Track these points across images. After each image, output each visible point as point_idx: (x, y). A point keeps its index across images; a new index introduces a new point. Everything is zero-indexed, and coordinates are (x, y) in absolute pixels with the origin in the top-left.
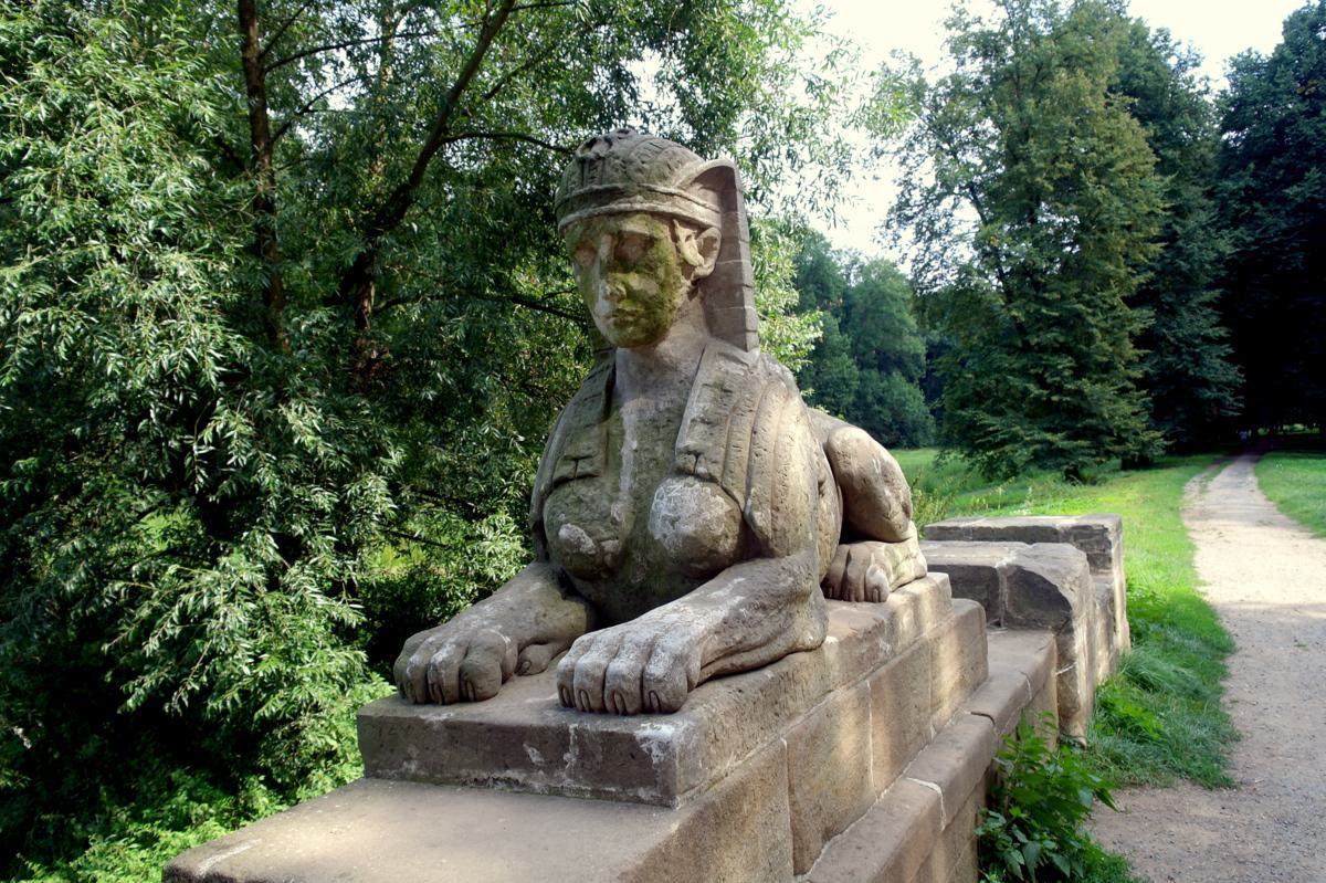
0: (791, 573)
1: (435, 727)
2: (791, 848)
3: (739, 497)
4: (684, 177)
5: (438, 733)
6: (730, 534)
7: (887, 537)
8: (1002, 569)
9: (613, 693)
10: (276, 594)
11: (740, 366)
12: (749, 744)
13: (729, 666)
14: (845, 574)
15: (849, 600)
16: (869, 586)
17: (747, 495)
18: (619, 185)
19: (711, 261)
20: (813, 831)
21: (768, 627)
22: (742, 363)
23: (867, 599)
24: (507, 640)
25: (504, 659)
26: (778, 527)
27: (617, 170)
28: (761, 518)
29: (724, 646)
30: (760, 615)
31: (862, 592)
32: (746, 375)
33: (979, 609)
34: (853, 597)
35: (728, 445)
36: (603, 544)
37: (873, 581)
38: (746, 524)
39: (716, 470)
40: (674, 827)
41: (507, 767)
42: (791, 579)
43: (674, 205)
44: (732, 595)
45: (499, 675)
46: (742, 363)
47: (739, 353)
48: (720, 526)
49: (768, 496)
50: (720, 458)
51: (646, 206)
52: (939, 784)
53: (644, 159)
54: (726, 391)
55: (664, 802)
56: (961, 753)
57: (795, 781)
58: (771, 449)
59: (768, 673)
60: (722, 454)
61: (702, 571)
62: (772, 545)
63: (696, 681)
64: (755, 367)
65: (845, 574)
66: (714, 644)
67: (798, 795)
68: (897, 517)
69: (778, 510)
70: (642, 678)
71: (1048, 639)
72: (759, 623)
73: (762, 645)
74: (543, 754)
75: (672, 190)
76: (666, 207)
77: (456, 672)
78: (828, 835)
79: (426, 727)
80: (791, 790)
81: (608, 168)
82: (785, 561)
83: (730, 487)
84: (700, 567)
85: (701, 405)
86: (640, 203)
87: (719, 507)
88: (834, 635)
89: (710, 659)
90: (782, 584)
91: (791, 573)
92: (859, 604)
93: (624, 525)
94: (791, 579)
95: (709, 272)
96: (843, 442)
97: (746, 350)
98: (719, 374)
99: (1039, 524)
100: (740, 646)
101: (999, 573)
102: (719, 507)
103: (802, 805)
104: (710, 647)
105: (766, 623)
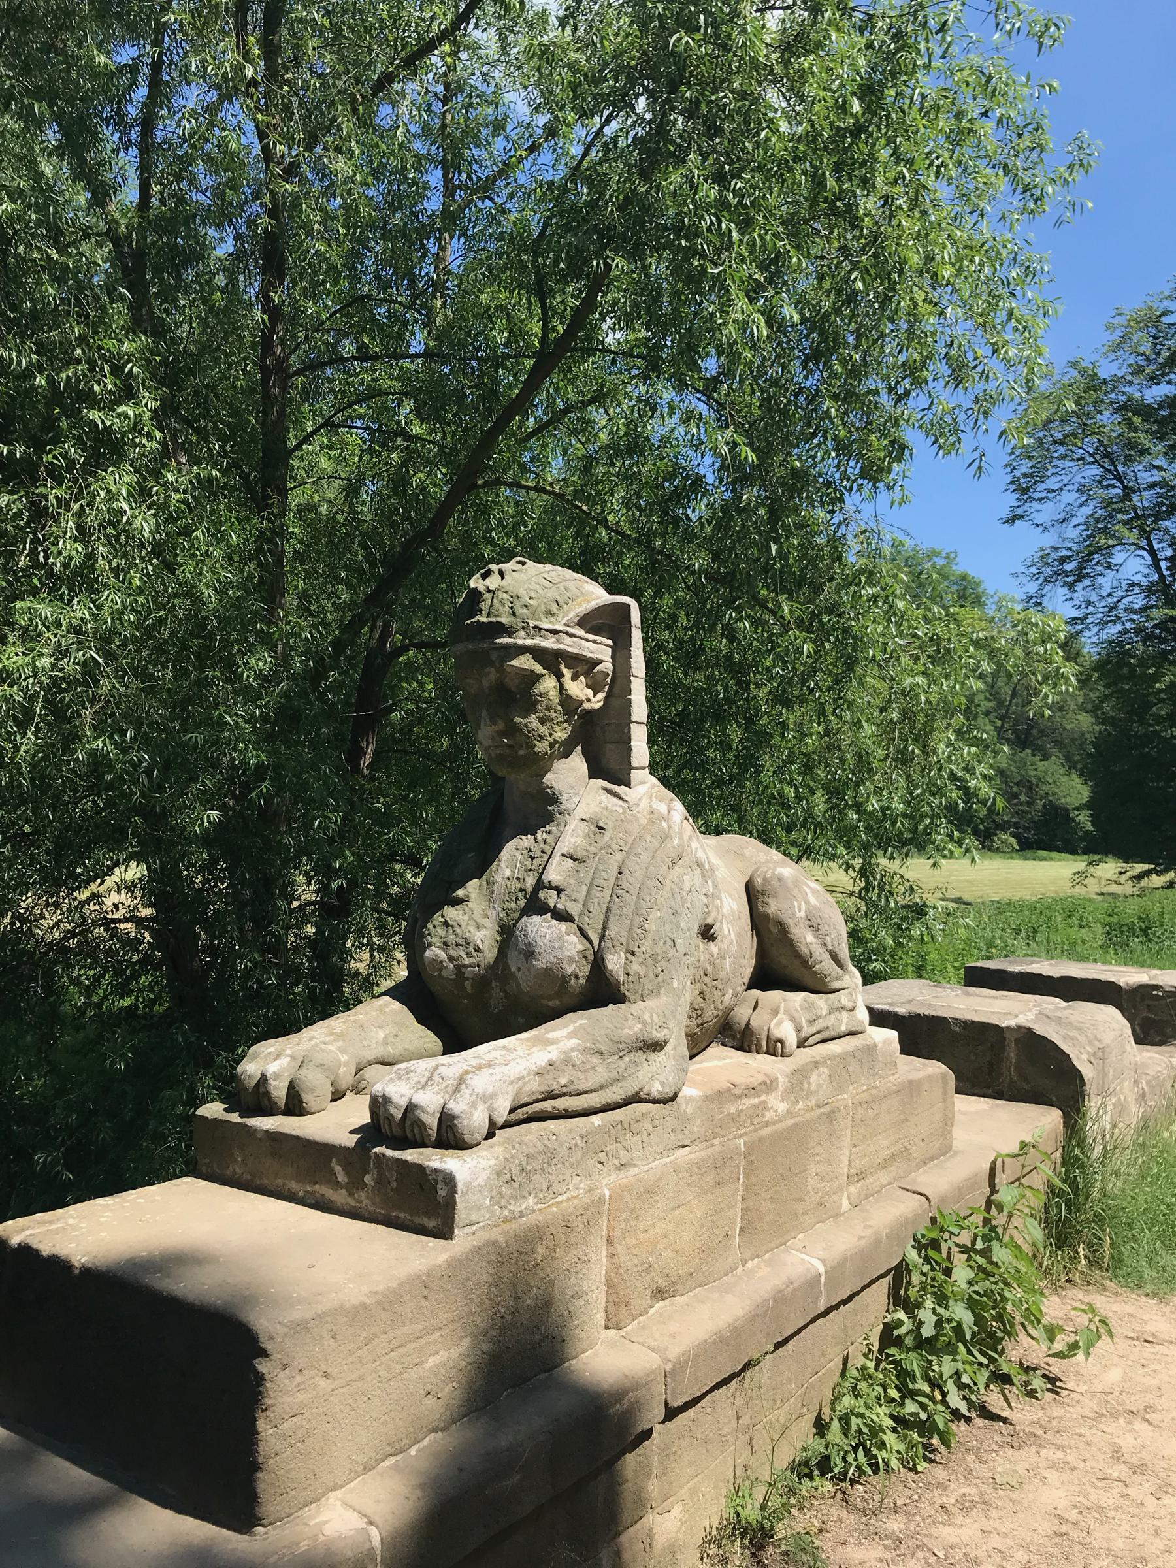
0: (640, 1019)
1: (259, 1136)
2: (604, 1301)
3: (596, 942)
4: (572, 615)
5: (260, 1140)
6: (580, 975)
7: (809, 981)
8: (1008, 1028)
9: (412, 1125)
10: (500, 774)
11: (620, 802)
12: (556, 1188)
13: (551, 1110)
14: (748, 1023)
15: (750, 1051)
16: (772, 1037)
17: (602, 938)
18: (504, 620)
19: (601, 696)
20: (639, 1290)
21: (602, 1074)
22: (621, 799)
23: (767, 1053)
24: (344, 1058)
25: (337, 1076)
26: (631, 972)
27: (503, 605)
28: (614, 963)
29: (543, 1089)
30: (595, 1060)
31: (764, 1044)
32: (624, 812)
33: (944, 1076)
34: (754, 1047)
35: (591, 883)
36: (463, 970)
37: (777, 1033)
38: (598, 964)
39: (574, 909)
40: (442, 1258)
41: (316, 1183)
42: (640, 1026)
43: (558, 641)
44: (568, 1037)
45: (328, 1091)
46: (621, 799)
47: (621, 790)
48: (570, 965)
49: (624, 940)
50: (581, 897)
51: (528, 642)
52: (824, 1261)
53: (533, 595)
54: (600, 828)
55: (444, 1232)
56: (868, 1232)
57: (617, 1234)
58: (634, 892)
59: (596, 1120)
60: (584, 893)
61: (553, 1009)
62: (623, 990)
63: (500, 1121)
64: (637, 805)
65: (748, 1023)
66: (535, 1086)
67: (619, 1248)
68: (825, 965)
69: (633, 954)
70: (442, 1113)
71: (1049, 1119)
72: (593, 1068)
73: (602, 1087)
74: (347, 1173)
75: (559, 627)
76: (549, 643)
77: (286, 1084)
78: (660, 1294)
79: (251, 1131)
80: (610, 1241)
81: (496, 602)
82: (636, 1008)
83: (586, 927)
84: (551, 1004)
85: (573, 840)
86: (522, 640)
87: (572, 945)
88: (695, 1084)
89: (526, 1100)
90: (626, 1031)
91: (640, 1019)
92: (759, 1057)
93: (487, 953)
94: (640, 1026)
95: (597, 706)
96: (765, 879)
97: (629, 787)
98: (598, 810)
99: (1102, 977)
100: (565, 1090)
101: (1007, 1035)
102: (572, 945)
103: (623, 1259)
104: (528, 1088)
105: (600, 1069)
